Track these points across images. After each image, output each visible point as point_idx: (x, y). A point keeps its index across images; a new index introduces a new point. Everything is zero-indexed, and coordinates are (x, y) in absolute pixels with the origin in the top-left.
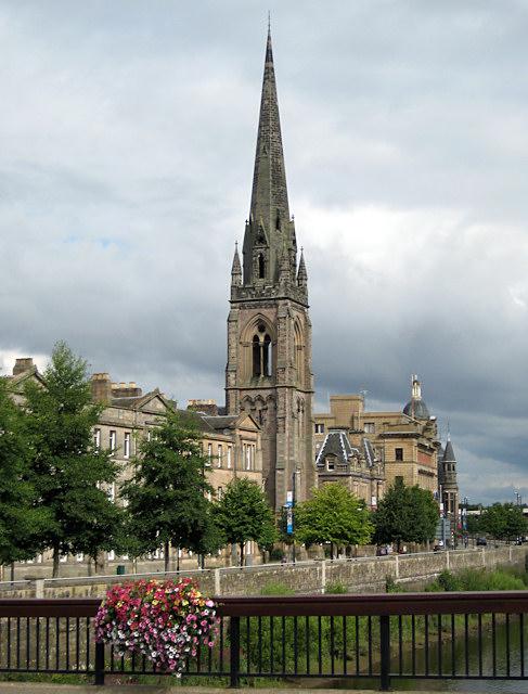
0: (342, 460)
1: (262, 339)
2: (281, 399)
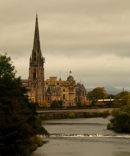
0: (50, 92)
1: (35, 72)
2: (38, 83)
